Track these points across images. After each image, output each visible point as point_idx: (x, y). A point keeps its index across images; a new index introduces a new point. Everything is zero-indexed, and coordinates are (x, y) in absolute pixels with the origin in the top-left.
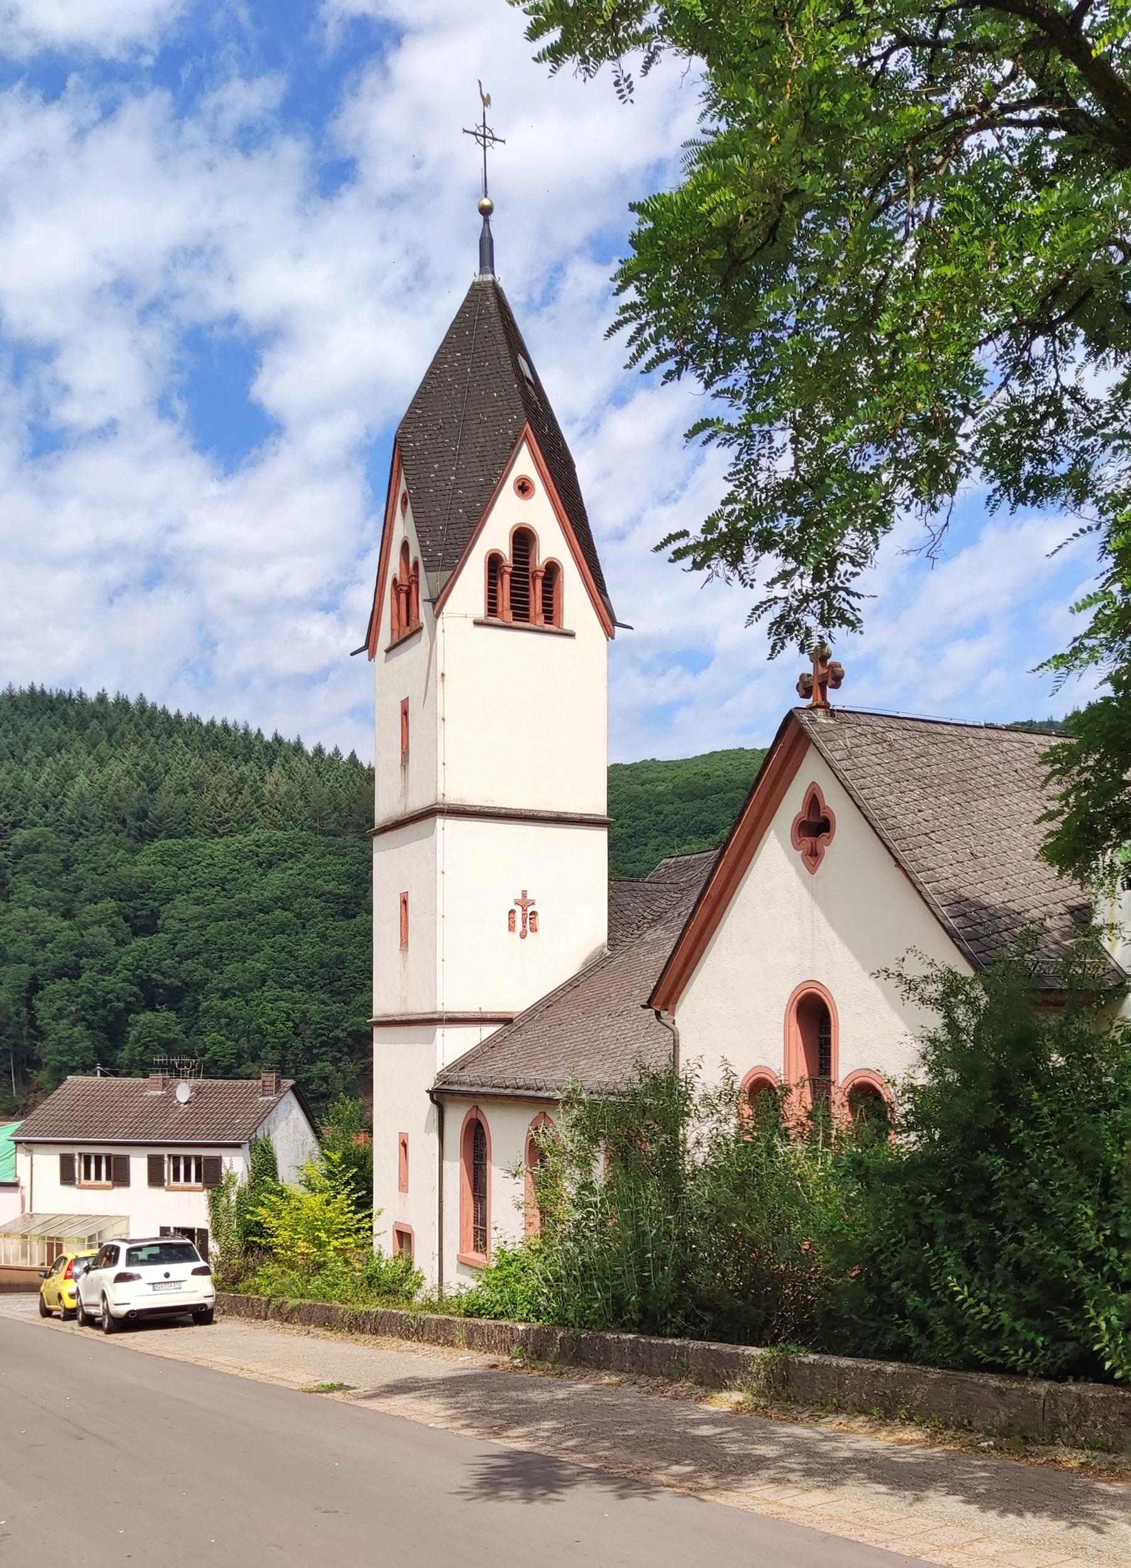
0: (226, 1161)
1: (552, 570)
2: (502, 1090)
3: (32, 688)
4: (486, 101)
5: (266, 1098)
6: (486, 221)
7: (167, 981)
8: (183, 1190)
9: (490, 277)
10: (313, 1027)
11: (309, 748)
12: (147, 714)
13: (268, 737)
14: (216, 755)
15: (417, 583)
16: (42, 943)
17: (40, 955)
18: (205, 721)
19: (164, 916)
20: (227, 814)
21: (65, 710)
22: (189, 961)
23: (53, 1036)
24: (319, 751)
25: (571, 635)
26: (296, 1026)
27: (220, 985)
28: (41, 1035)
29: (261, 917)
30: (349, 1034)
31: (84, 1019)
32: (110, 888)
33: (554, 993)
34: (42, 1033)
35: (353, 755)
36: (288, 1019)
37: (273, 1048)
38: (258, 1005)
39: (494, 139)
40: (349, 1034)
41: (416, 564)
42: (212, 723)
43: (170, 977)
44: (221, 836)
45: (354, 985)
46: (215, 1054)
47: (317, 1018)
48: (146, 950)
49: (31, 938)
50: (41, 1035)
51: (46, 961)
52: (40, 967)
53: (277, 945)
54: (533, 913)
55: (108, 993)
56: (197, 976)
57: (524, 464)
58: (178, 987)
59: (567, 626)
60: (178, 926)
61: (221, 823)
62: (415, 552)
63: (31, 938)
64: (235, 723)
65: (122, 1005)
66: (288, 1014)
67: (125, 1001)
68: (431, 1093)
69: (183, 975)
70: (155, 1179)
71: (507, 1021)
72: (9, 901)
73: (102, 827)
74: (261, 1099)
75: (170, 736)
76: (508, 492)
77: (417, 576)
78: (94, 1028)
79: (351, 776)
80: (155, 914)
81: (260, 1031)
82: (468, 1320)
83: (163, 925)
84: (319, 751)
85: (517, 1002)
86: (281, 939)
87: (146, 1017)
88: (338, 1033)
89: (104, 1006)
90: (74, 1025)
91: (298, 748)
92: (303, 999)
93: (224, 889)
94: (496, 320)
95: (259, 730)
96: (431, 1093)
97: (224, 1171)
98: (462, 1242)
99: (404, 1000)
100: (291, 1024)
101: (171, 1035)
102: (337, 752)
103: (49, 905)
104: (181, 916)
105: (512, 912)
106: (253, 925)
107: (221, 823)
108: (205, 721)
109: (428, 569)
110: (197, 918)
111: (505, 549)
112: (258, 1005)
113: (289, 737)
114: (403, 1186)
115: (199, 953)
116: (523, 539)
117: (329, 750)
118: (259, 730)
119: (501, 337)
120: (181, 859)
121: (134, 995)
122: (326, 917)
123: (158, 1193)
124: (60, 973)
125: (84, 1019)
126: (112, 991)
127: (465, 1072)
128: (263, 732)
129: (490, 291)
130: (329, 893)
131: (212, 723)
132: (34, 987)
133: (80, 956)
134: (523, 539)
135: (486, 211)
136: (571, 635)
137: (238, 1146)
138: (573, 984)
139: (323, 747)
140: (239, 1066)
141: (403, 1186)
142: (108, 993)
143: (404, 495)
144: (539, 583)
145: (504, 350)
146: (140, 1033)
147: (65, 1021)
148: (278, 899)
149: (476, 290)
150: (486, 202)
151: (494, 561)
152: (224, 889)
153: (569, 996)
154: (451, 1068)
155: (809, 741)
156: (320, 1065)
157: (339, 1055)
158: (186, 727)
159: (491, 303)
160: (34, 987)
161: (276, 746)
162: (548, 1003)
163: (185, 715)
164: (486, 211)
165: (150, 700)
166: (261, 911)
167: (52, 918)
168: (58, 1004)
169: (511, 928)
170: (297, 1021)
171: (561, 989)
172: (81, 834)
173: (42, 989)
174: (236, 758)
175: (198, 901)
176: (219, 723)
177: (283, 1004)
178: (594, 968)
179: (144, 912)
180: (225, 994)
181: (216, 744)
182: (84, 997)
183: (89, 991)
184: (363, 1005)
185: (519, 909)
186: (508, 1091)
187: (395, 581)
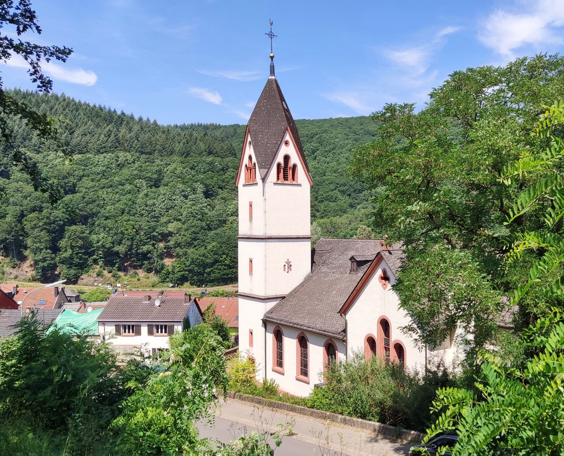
0: (176, 327)
1: (295, 166)
2: (289, 324)
3: (15, 89)
4: (272, 24)
5: (186, 304)
6: (272, 60)
7: (81, 213)
8: (160, 336)
9: (273, 77)
10: (144, 231)
11: (136, 117)
12: (66, 101)
13: (119, 113)
14: (98, 120)
15: (255, 169)
16: (26, 197)
17: (25, 202)
18: (92, 105)
19: (78, 186)
20: (104, 145)
21: (30, 98)
22: (90, 205)
23: (32, 235)
24: (141, 119)
25: (300, 185)
26: (137, 231)
27: (104, 215)
28: (26, 235)
29: (120, 187)
30: (159, 234)
31: (45, 229)
32: (130, 236)
33: (296, 288)
34: (27, 234)
35: (155, 121)
36: (133, 229)
37: (128, 240)
38: (121, 223)
39: (274, 36)
40: (159, 234)
41: (255, 164)
42: (95, 106)
43: (82, 211)
44: (102, 153)
45: (160, 214)
46: (103, 242)
47: (146, 228)
48: (72, 200)
49: (20, 195)
50: (26, 235)
51: (28, 204)
52: (24, 207)
53: (128, 198)
54: (291, 265)
55: (56, 218)
56: (94, 210)
57: (288, 137)
58: (85, 215)
59: (299, 182)
60: (84, 190)
61: (101, 148)
62: (254, 160)
63: (20, 195)
64: (104, 106)
65: (62, 222)
66: (134, 226)
67: (63, 221)
68: (263, 320)
69: (88, 210)
70: (150, 333)
71: (284, 298)
72: (10, 179)
73: (49, 148)
74: (185, 304)
75: (77, 111)
76: (283, 146)
77: (255, 167)
78: (50, 232)
79: (155, 130)
80: (74, 185)
81: (122, 233)
82: (311, 409)
83: (78, 190)
84: (141, 119)
85: (285, 291)
86: (129, 196)
87: (74, 227)
88: (155, 234)
89: (54, 223)
90: (41, 231)
91: (132, 118)
92: (139, 220)
93: (104, 175)
94: (276, 91)
95: (115, 109)
96: (263, 320)
97: (175, 330)
98: (274, 363)
99: (251, 290)
100: (135, 230)
101: (85, 235)
102: (148, 120)
103: (27, 181)
104: (86, 186)
105: (285, 265)
106: (117, 190)
107: (101, 148)
108: (92, 105)
109: (260, 168)
110: (93, 187)
111: (282, 162)
112: (121, 223)
113: (128, 113)
114: (251, 343)
115: (95, 201)
116: (287, 158)
117: (145, 119)
118: (115, 109)
119: (278, 97)
120: (85, 163)
121: (67, 218)
122: (147, 187)
123: (151, 337)
124: (33, 210)
125: (45, 229)
126: (58, 217)
127: (273, 314)
128: (116, 110)
129: (274, 82)
130: (149, 177)
131: (95, 106)
132: (23, 215)
133: (42, 202)
134: (287, 158)
135: (272, 58)
136: (300, 185)
137: (180, 322)
138: (302, 285)
139: (142, 117)
140: (113, 247)
141: (251, 343)
142: (56, 218)
143: (250, 142)
144: (291, 170)
145: (279, 101)
146: (71, 234)
147: (37, 229)
148: (128, 180)
149: (270, 81)
150: (272, 55)
151: (279, 165)
152: (104, 175)
153: (302, 289)
154: (268, 313)
155: (383, 259)
156: (147, 246)
157: (155, 242)
158: (84, 107)
159: (275, 85)
160: (23, 215)
161: (122, 116)
162: (295, 291)
163: (83, 102)
164: (272, 58)
165: (67, 95)
166: (120, 185)
167: (29, 186)
168: (34, 222)
169: (284, 270)
170: (137, 229)
171: (299, 286)
172: (40, 151)
173: (26, 216)
174: (106, 121)
175: (93, 180)
176: (97, 106)
177: (131, 222)
178: (308, 279)
179: (69, 184)
180: (107, 218)
181: (97, 115)
182: (45, 219)
183: (48, 218)
184: (164, 223)
185: (286, 265)
186: (291, 325)
187: (246, 166)
